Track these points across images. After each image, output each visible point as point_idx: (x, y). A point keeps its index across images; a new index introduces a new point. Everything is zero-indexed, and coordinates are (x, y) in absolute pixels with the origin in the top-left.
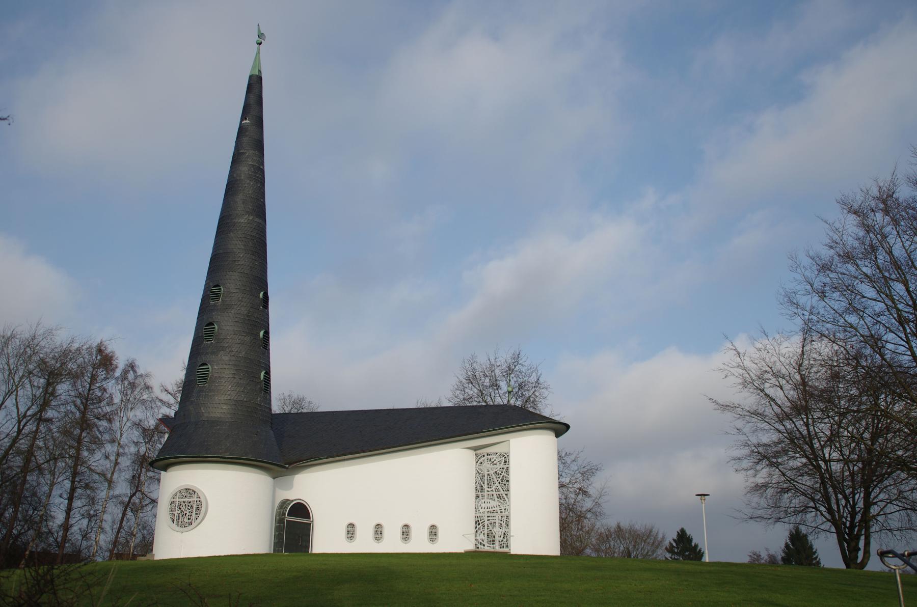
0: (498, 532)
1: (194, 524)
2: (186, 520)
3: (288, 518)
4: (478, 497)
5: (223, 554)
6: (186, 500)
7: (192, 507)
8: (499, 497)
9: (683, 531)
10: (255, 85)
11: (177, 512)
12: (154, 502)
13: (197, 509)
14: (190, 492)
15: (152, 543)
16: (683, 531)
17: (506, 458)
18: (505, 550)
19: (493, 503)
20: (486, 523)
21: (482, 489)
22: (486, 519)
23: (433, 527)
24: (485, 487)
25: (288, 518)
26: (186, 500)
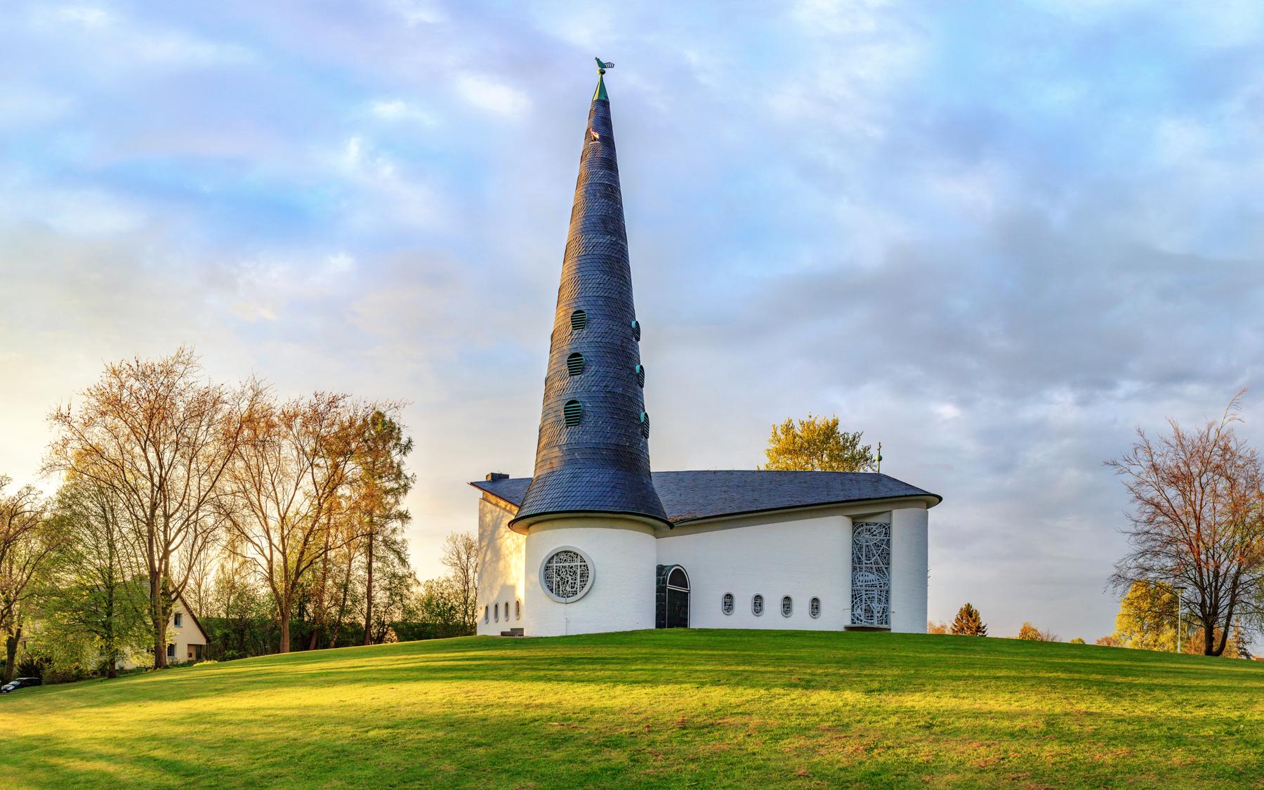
0: (876, 606)
1: (580, 595)
2: (568, 589)
3: (669, 587)
4: (854, 569)
5: (650, 441)
6: (566, 564)
7: (575, 573)
8: (878, 570)
9: (969, 606)
10: (602, 104)
12: (836, 711)
13: (582, 576)
14: (569, 554)
15: (856, 564)
16: (969, 606)
17: (887, 529)
18: (884, 626)
19: (871, 577)
21: (860, 562)
23: (787, 599)
24: (863, 559)
25: (669, 587)
26: (566, 564)
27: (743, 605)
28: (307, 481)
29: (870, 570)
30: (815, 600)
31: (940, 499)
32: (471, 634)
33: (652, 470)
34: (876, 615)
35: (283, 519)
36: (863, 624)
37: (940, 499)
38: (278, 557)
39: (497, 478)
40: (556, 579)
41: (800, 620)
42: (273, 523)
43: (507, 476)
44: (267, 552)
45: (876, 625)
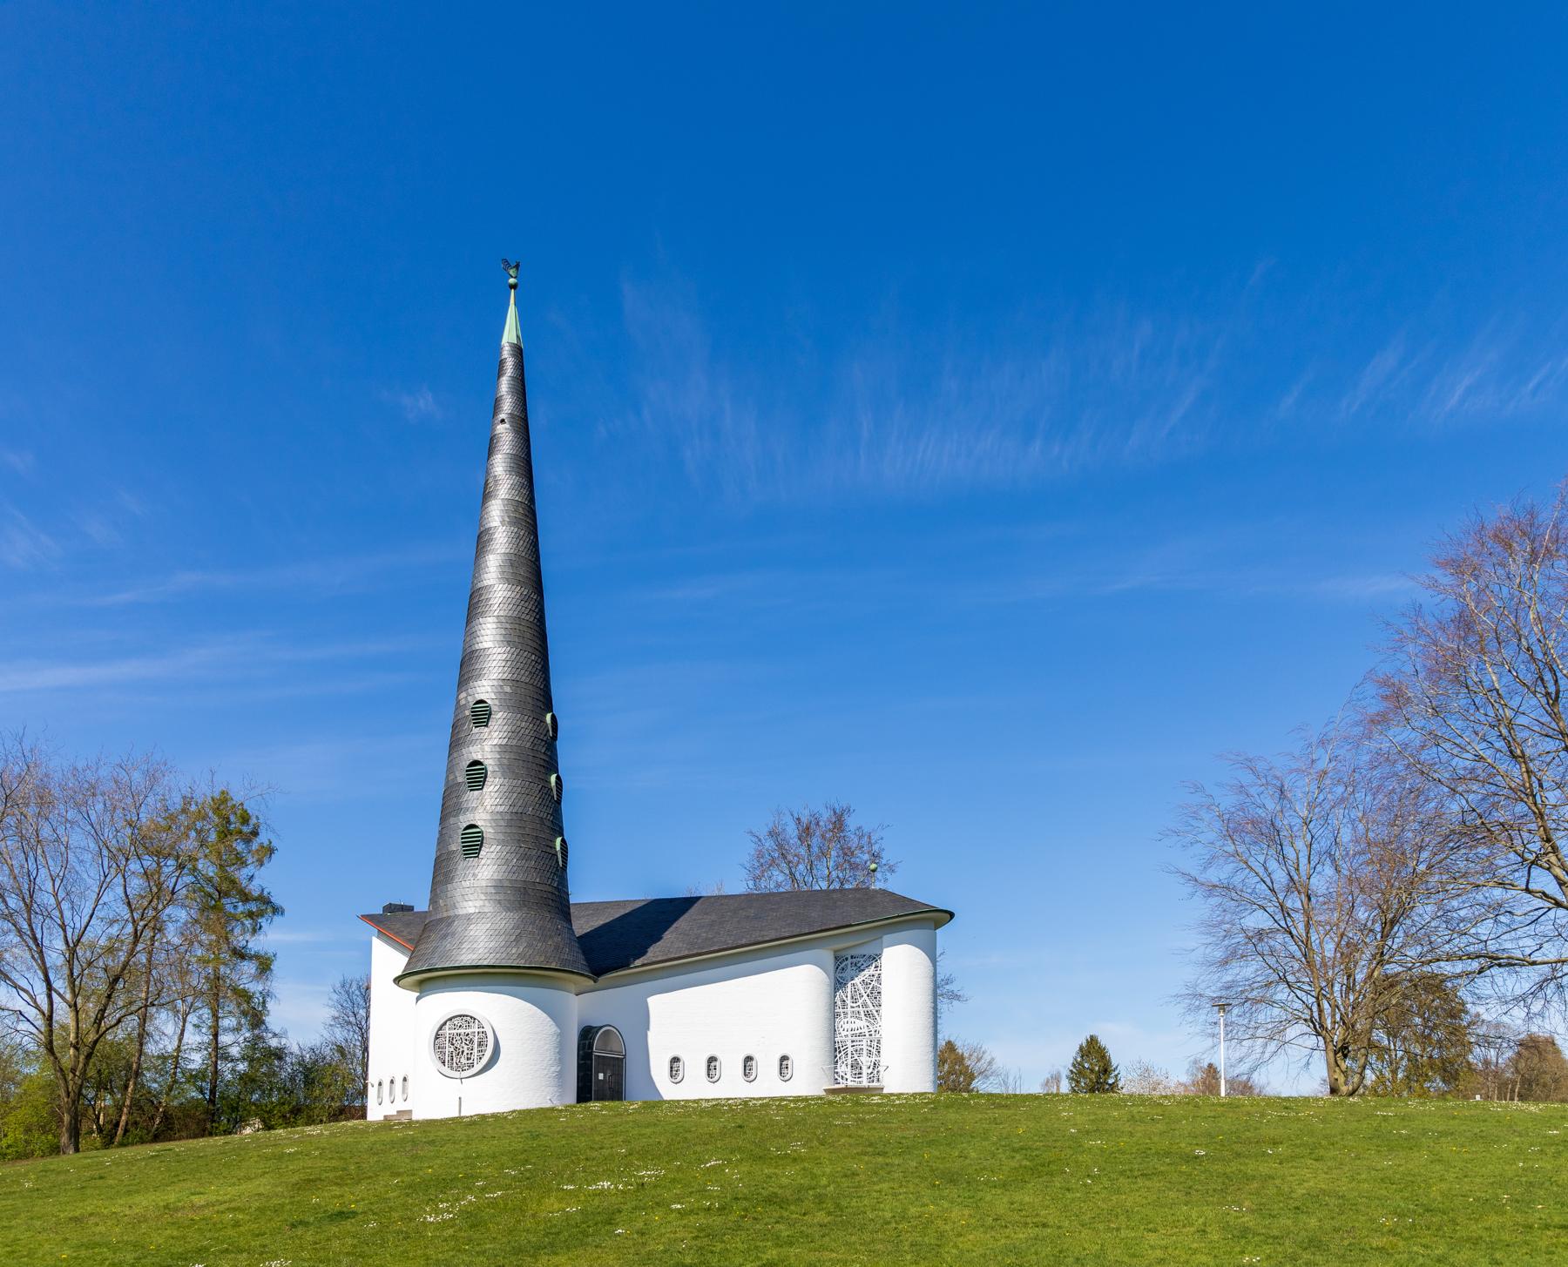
0: (865, 1060)
2: (464, 1061)
6: (462, 1031)
8: (868, 1014)
11: (449, 1049)
13: (480, 1044)
18: (875, 1084)
19: (859, 1023)
20: (850, 1049)
22: (849, 1044)
24: (849, 1001)
26: (462, 1031)
27: (767, 1067)
28: (113, 896)
29: (857, 1015)
30: (712, 1059)
31: (952, 915)
32: (341, 1113)
33: (574, 899)
34: (865, 1071)
35: (73, 952)
36: (850, 1084)
37: (952, 915)
38: (63, 1013)
39: (390, 908)
40: (449, 1049)
41: (768, 1086)
42: (55, 958)
43: (411, 908)
44: (42, 1000)
45: (865, 1083)
